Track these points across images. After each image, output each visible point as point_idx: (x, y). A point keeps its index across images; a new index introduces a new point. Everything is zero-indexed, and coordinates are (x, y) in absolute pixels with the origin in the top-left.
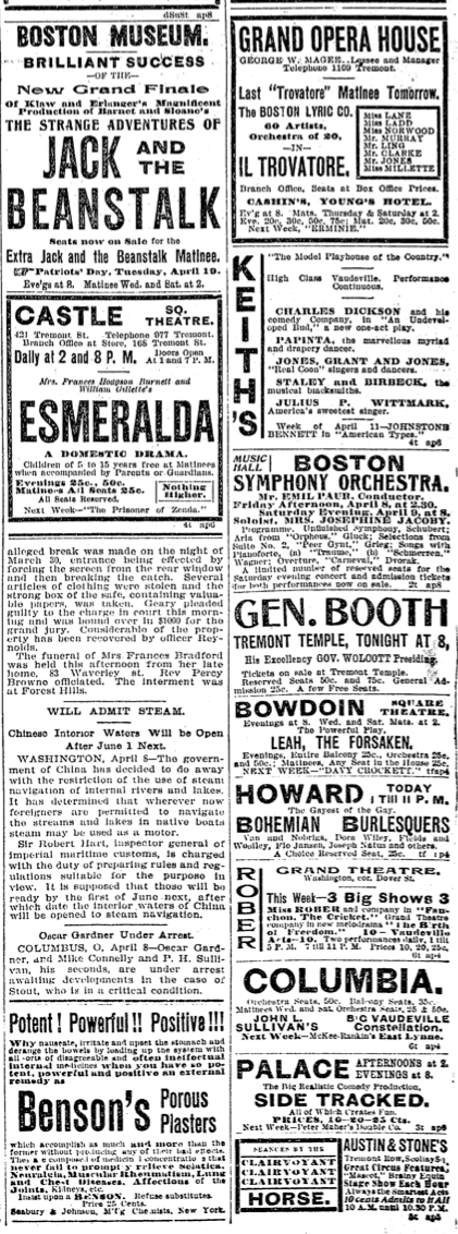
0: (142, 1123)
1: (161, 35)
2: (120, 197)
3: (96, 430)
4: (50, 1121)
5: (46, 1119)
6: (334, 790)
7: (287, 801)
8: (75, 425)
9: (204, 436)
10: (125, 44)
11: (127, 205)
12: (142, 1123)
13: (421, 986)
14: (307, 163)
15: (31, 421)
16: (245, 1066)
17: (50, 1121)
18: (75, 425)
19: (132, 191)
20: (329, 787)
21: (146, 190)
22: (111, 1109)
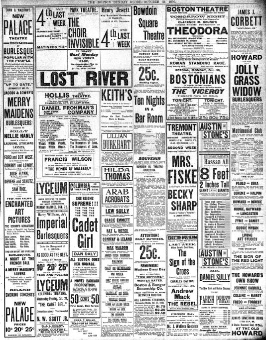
0: (130, 98)
2: (186, 77)
4: (93, 228)
5: (92, 227)
7: (243, 59)
10: (13, 106)
11: (188, 79)
12: (130, 98)
17: (93, 228)
19: (189, 75)
20: (254, 56)
22: (88, 229)
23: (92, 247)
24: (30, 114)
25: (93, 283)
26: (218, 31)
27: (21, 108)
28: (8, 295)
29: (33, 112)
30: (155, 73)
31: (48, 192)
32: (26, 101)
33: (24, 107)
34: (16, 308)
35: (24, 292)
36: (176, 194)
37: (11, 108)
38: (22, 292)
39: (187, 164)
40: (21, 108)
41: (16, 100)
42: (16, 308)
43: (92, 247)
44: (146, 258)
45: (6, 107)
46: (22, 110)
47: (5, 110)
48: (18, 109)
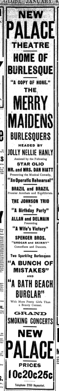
1: (36, 219)
3: (26, 154)
6: (25, 364)
8: (27, 58)
9: (44, 286)
13: (31, 46)
14: (25, 282)
15: (27, 136)
16: (21, 364)
18: (27, 58)
20: (28, 163)
21: (28, 269)
23: (44, 109)
24: (48, 121)
25: (47, 124)
26: (42, 45)
27: (33, 112)
28: (12, 321)
29: (52, 120)
30: (27, 319)
31: (32, 322)
32: (41, 102)
33: (37, 111)
34: (25, 342)
35: (37, 317)
36: (41, 284)
37: (18, 112)
38: (33, 317)
39: (31, 134)
40: (33, 112)
41: (26, 100)
42: (25, 342)
43: (44, 109)
44: (33, 73)
45: (11, 110)
46: (36, 115)
47: (10, 115)
48: (30, 115)
